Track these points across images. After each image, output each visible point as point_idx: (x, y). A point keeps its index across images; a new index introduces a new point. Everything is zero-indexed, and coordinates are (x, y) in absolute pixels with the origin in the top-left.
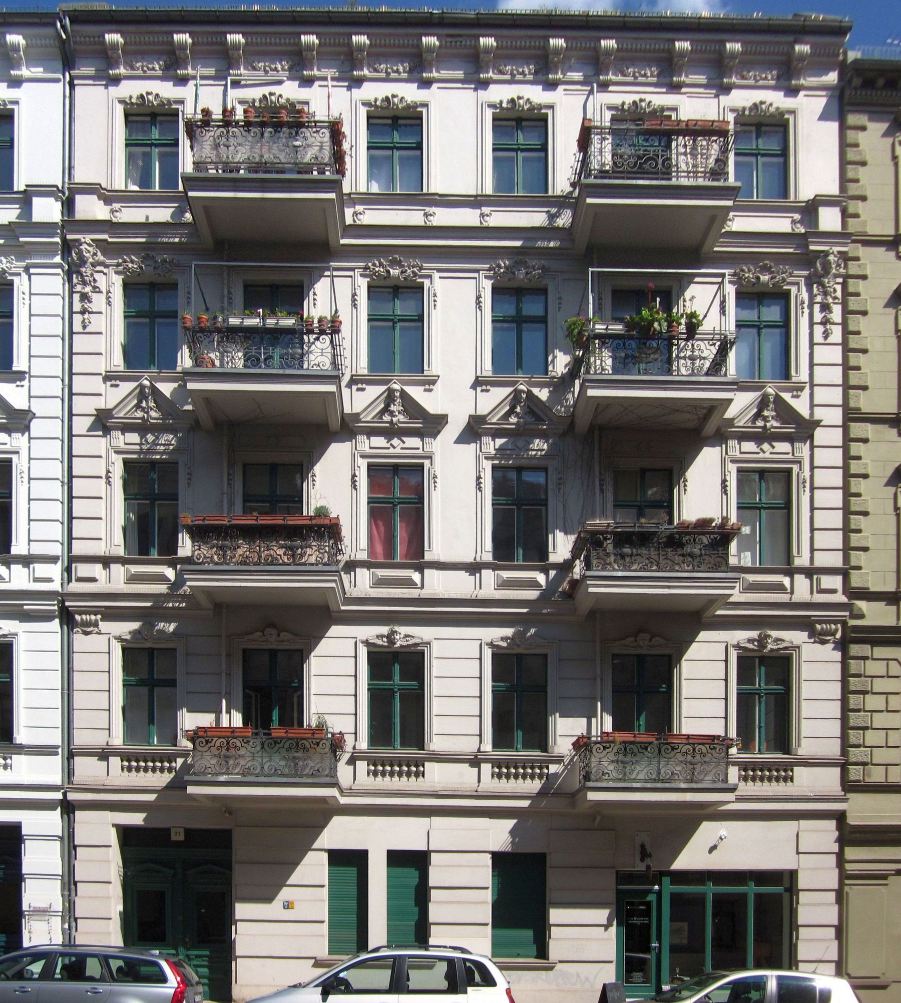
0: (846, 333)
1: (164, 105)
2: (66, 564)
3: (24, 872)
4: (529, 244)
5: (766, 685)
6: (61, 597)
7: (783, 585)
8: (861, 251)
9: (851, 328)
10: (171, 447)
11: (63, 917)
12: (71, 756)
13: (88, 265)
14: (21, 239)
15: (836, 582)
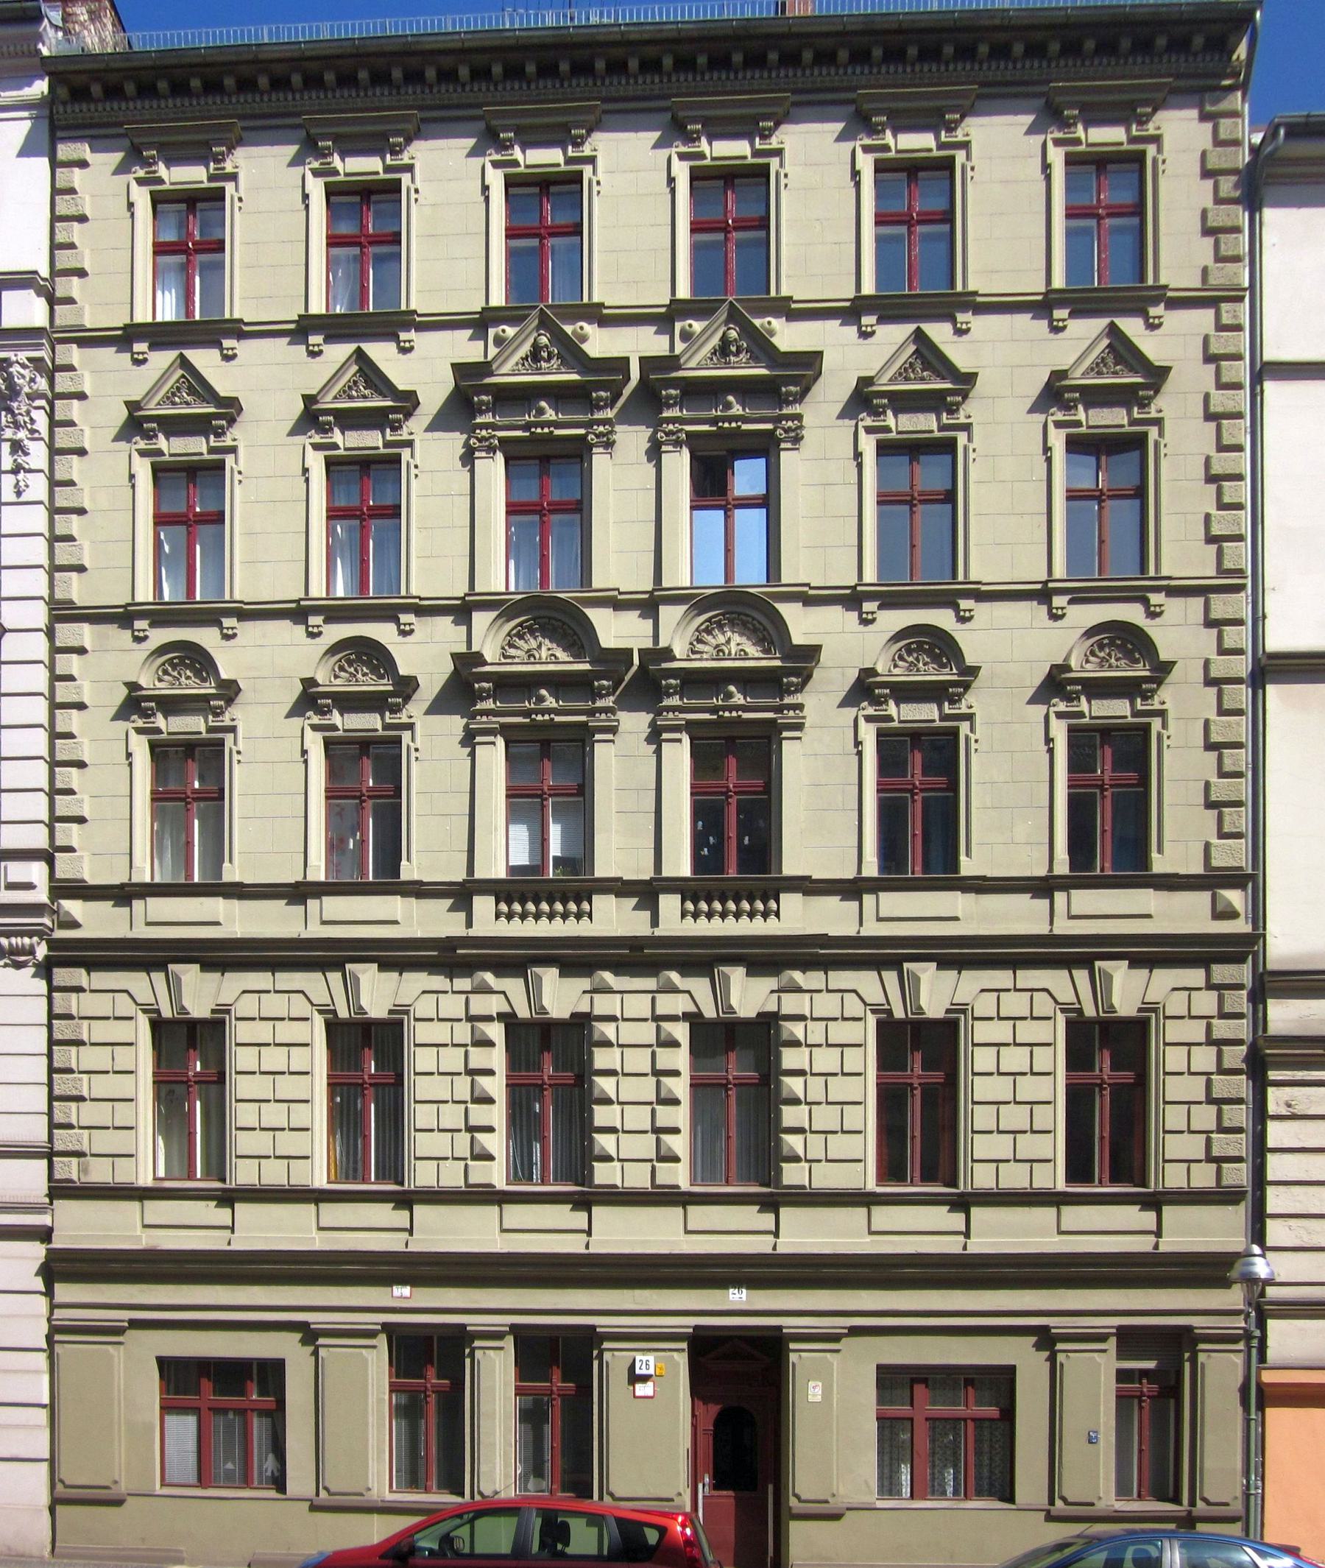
0: (54, 483)
8: (74, 354)
9: (59, 476)
13: (23, 397)
15: (36, 872)
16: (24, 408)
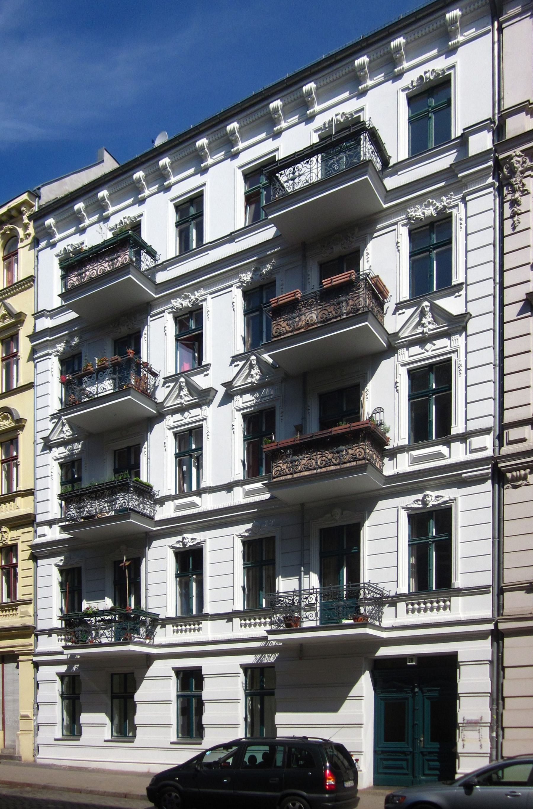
1: (439, 75)
2: (497, 433)
3: (459, 691)
4: (71, 331)
5: (432, 534)
6: (494, 461)
7: (441, 453)
10: (271, 397)
11: (491, 728)
12: (501, 591)
13: (518, 173)
14: (459, 175)
16: (518, 180)
